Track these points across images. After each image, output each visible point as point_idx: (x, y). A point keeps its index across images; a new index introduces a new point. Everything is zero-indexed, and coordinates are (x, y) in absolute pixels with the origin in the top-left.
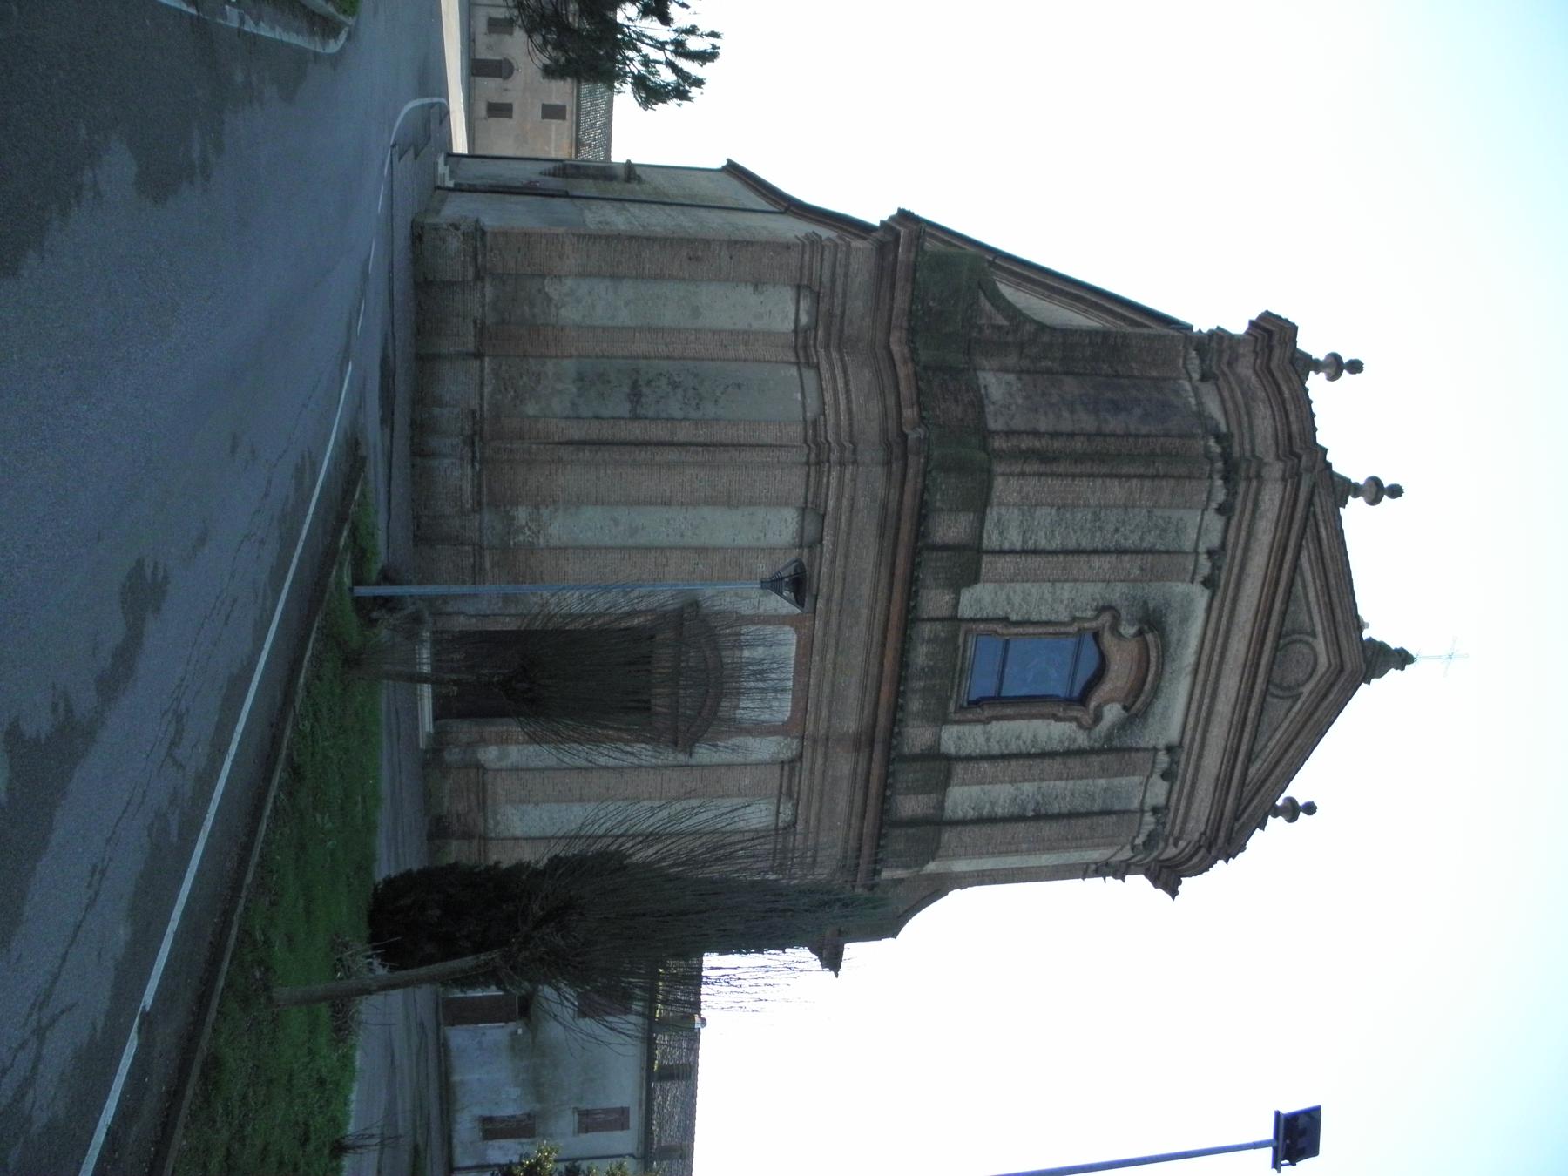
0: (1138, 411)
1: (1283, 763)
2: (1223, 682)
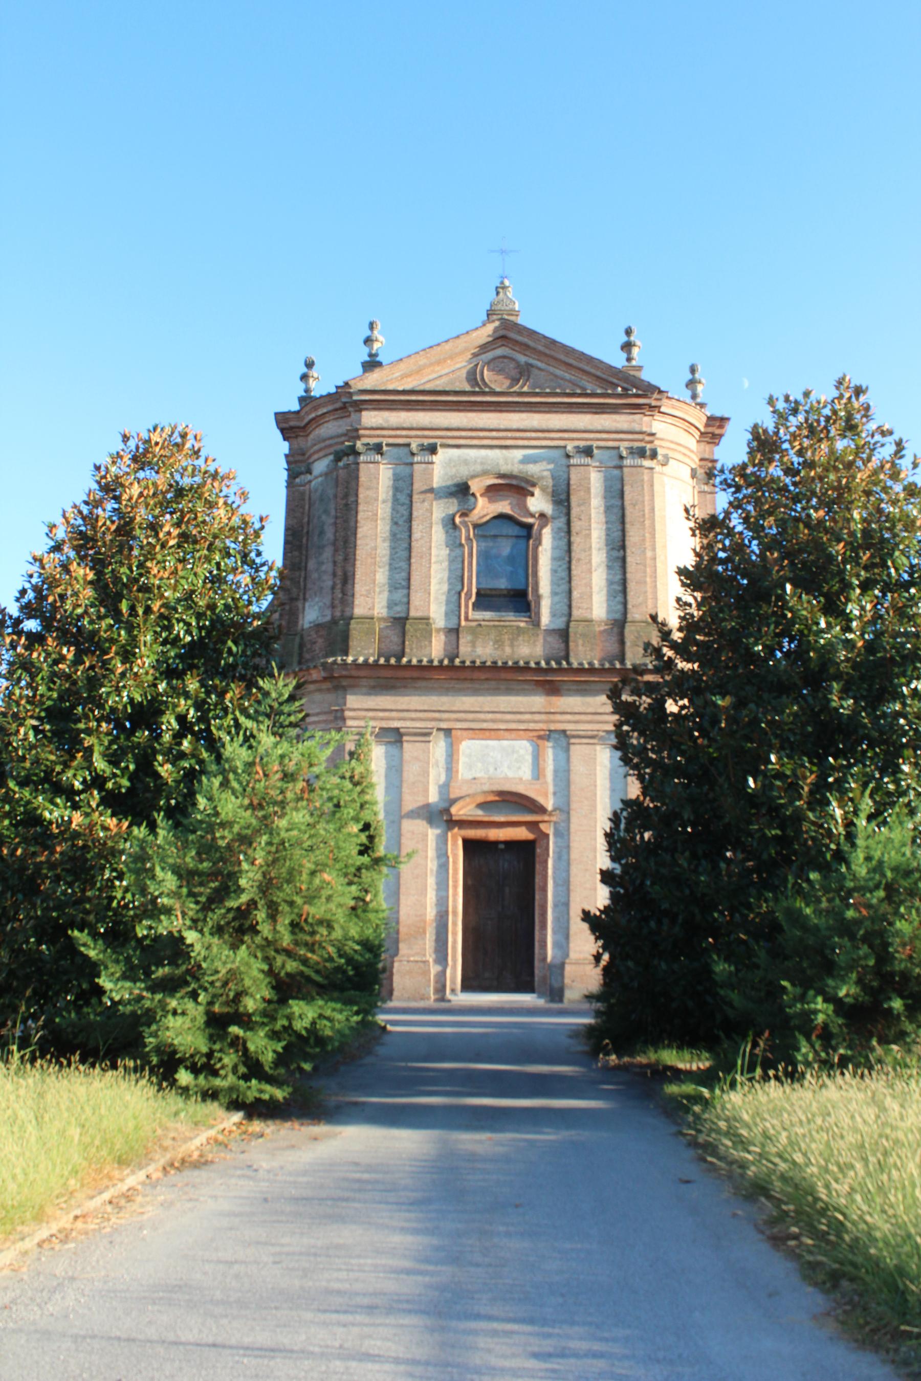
0: (324, 517)
1: (581, 365)
2: (515, 426)
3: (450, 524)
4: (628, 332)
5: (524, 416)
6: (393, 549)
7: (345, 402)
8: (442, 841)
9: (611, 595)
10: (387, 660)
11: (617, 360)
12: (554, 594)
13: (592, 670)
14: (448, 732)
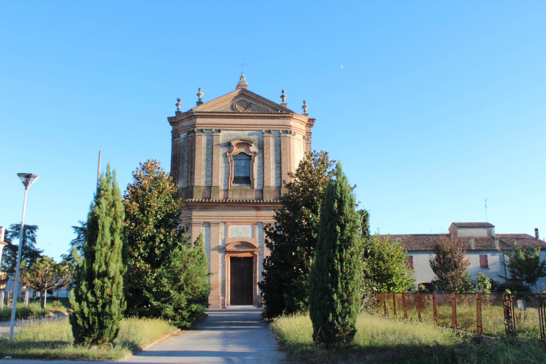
2: (246, 123)
3: (225, 156)
4: (283, 92)
5: (249, 120)
6: (207, 164)
7: (191, 115)
8: (223, 258)
9: (277, 179)
10: (205, 200)
11: (279, 101)
12: (258, 178)
13: (270, 203)
14: (225, 223)
